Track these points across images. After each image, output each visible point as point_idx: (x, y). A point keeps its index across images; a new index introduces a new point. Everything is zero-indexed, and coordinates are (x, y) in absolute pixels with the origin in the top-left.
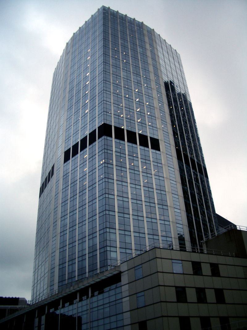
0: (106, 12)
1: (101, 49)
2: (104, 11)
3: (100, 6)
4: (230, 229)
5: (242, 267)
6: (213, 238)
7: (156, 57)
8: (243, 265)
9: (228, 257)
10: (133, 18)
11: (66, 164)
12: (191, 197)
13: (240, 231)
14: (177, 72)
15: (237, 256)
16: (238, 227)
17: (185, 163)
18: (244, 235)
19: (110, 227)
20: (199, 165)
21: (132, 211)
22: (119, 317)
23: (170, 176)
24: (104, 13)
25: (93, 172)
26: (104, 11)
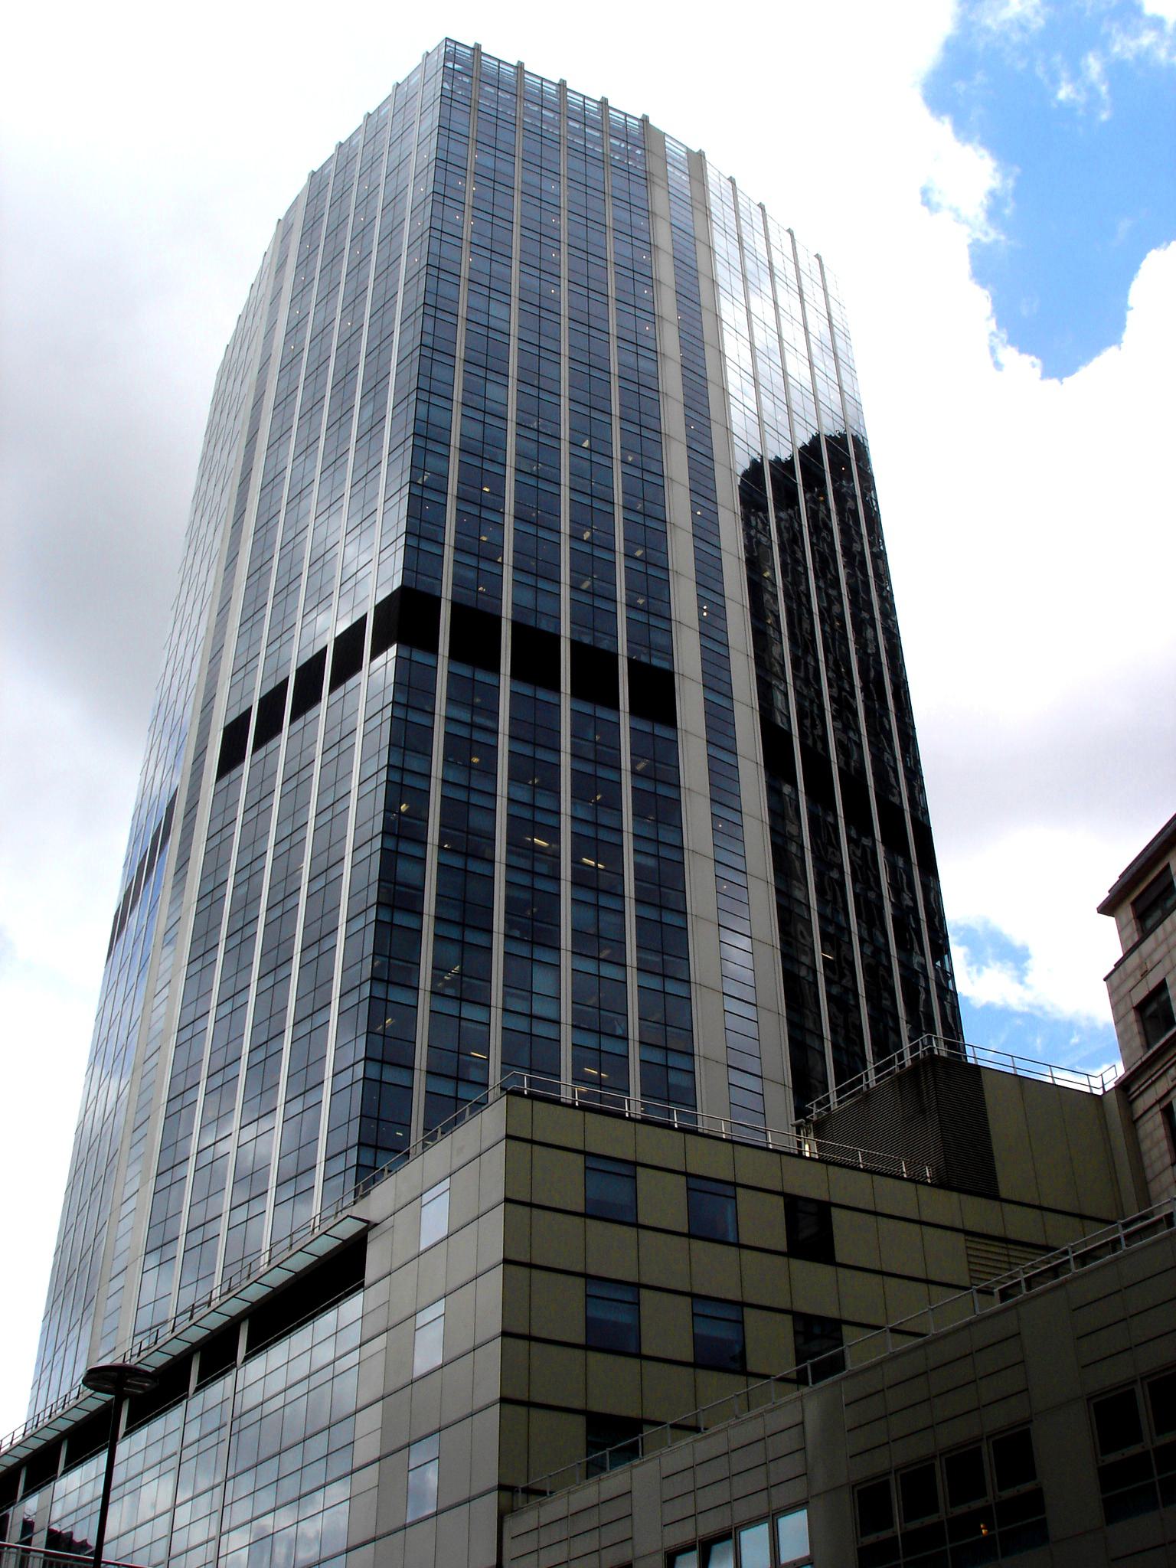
0: (456, 66)
1: (419, 241)
2: (450, 65)
3: (431, 41)
4: (921, 1056)
5: (962, 1237)
6: (847, 1104)
7: (704, 284)
8: (969, 1227)
9: (897, 1182)
10: (599, 99)
11: (225, 781)
12: (866, 981)
13: (977, 1069)
14: (841, 388)
15: (942, 1183)
16: (969, 1051)
17: (883, 842)
18: (986, 1078)
19: (387, 1058)
20: (891, 814)
21: (505, 994)
22: (341, 1435)
23: (739, 859)
24: (449, 75)
25: (336, 813)
26: (450, 65)
